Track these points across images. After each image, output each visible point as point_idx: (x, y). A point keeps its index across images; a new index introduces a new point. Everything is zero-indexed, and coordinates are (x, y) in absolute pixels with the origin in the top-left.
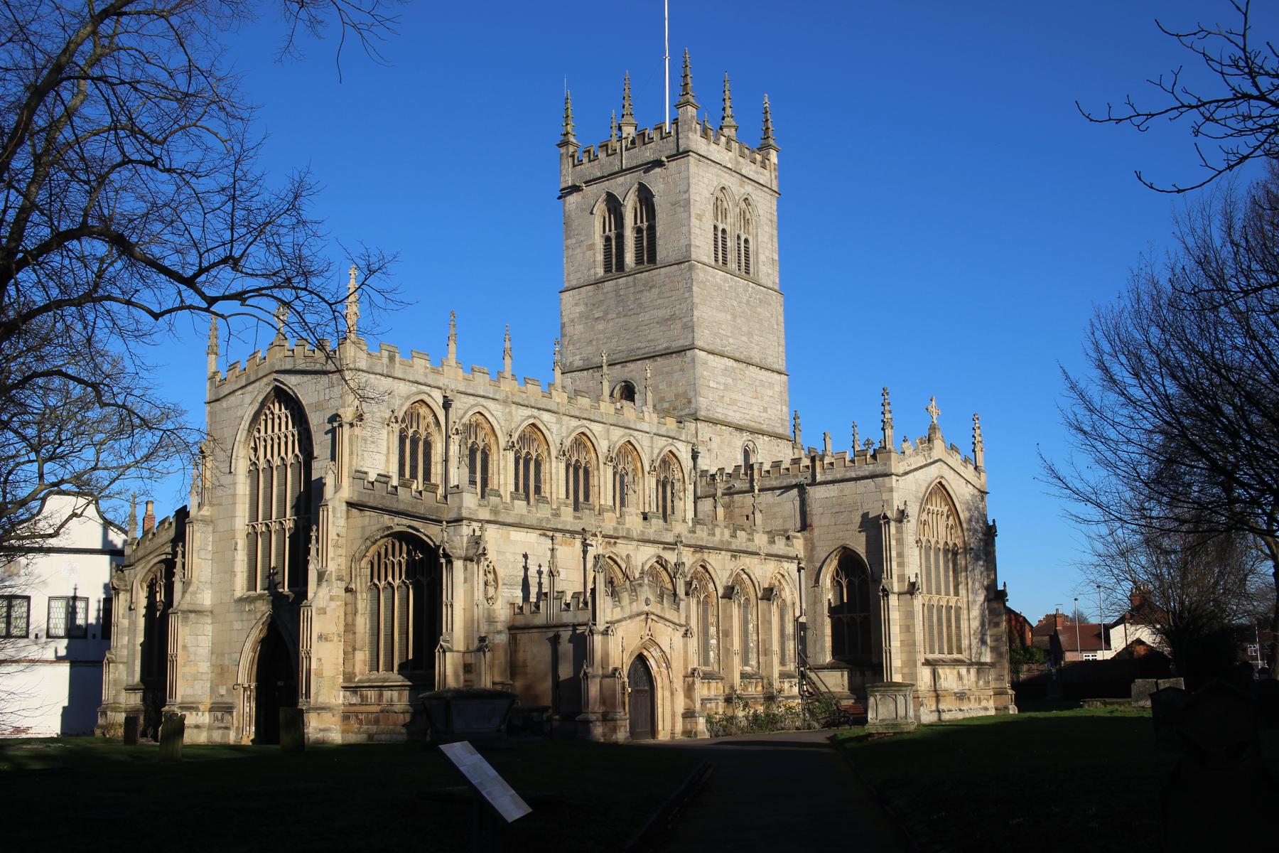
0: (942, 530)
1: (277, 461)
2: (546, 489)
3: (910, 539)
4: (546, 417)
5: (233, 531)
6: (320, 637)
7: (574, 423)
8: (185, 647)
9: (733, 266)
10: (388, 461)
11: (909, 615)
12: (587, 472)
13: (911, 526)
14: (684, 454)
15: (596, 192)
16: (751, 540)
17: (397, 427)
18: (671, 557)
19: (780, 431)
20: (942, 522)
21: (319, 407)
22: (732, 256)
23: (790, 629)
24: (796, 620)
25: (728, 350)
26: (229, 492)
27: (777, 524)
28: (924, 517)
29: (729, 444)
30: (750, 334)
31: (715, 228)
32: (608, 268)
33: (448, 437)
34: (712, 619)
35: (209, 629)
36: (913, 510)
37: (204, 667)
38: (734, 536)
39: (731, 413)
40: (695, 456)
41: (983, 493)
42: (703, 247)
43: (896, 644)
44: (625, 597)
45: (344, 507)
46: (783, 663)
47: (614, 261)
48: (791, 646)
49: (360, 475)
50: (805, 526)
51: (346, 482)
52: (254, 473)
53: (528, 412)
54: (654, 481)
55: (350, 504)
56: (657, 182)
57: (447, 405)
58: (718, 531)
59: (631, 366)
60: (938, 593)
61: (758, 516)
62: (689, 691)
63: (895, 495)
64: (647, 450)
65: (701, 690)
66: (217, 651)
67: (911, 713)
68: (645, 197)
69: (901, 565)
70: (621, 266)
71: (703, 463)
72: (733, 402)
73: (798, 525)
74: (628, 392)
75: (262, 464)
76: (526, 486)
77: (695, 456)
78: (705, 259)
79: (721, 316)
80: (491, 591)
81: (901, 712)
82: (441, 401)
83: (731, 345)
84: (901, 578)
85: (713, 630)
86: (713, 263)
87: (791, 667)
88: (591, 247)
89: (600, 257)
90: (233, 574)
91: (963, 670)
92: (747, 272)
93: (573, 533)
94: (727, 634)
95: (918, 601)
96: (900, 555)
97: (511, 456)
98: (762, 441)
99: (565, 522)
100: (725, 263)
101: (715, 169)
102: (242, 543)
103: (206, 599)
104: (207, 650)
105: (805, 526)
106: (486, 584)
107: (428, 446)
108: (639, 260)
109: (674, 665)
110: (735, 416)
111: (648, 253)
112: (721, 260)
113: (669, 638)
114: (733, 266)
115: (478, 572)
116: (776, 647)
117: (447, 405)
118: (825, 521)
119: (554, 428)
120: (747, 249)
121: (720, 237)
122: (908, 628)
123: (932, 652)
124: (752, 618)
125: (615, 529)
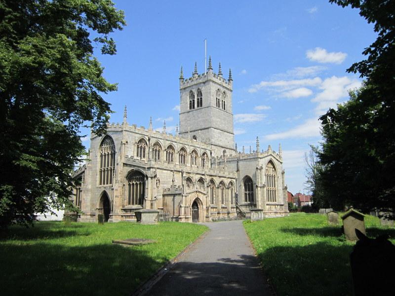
0: (271, 171)
1: (107, 153)
2: (161, 158)
3: (263, 174)
4: (174, 143)
5: (96, 170)
6: (116, 197)
7: (181, 145)
8: (84, 199)
9: (221, 108)
10: (134, 153)
11: (263, 192)
12: (184, 156)
13: (264, 170)
14: (209, 153)
15: (189, 90)
16: (224, 174)
17: (136, 145)
18: (203, 177)
19: (232, 148)
20: (271, 169)
21: (117, 139)
22: (221, 105)
23: (234, 195)
24: (235, 193)
25: (220, 128)
26: (95, 161)
27: (231, 170)
28: (267, 168)
29: (220, 151)
30: (225, 124)
31: (217, 98)
32: (190, 108)
33: (149, 148)
34: (214, 193)
35: (90, 195)
36: (264, 167)
37: (89, 204)
38: (220, 172)
39: (243, 163)
40: (211, 153)
41: (178, 219)
42: (214, 103)
43: (259, 196)
44: (191, 187)
45: (122, 164)
46: (232, 203)
47: (192, 106)
48: (234, 199)
49: (127, 157)
50: (238, 170)
51: (123, 158)
52: (101, 156)
53: (170, 142)
54: (201, 159)
55: (124, 164)
56: (203, 89)
57: (149, 140)
58: (216, 171)
59: (196, 132)
60: (270, 186)
61: (226, 168)
62: (207, 210)
63: (260, 163)
64: (199, 152)
65: (211, 210)
66: (92, 200)
67: (262, 217)
68: (200, 93)
69: (261, 180)
70: (194, 108)
71: (213, 155)
72: (221, 140)
73: (236, 170)
74: (195, 137)
75: (103, 154)
76: (169, 160)
77: (211, 153)
78: (214, 106)
79: (218, 120)
80: (158, 185)
81: (260, 217)
82: (148, 139)
83: (221, 127)
84: (261, 183)
85: (214, 196)
86: (216, 107)
87: (234, 205)
88: (187, 103)
89: (189, 106)
90: (96, 181)
91: (277, 206)
92: (225, 109)
93: (179, 172)
94: (218, 196)
95: (265, 189)
96: (261, 177)
97: (165, 152)
98: (227, 150)
99: (177, 169)
100: (219, 107)
101: (216, 85)
102: (98, 173)
103: (90, 187)
104: (90, 200)
105: (238, 170)
106: (157, 183)
107: (144, 149)
108: (198, 106)
109: (203, 204)
110: (221, 144)
111: (200, 103)
112: (218, 104)
113: (201, 197)
114: (221, 108)
115: (155, 180)
116: (230, 200)
117: (149, 140)
118: (243, 169)
119: (176, 146)
120: (224, 104)
121: (218, 101)
122: (263, 195)
123: (269, 201)
124: (224, 192)
125: (190, 170)
